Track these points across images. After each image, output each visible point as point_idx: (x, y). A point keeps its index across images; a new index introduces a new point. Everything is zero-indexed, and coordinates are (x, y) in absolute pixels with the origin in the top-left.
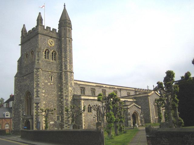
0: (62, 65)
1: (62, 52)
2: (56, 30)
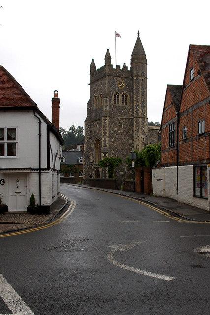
0: (133, 110)
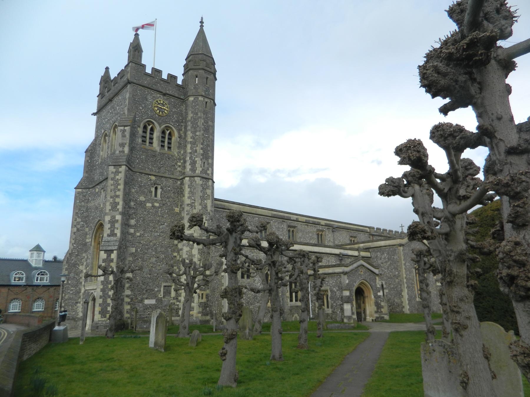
1: (187, 131)
2: (175, 78)
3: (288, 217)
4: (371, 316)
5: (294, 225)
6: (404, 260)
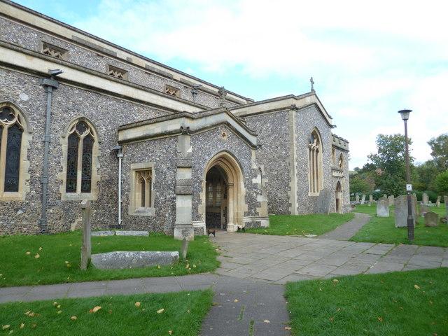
3: (110, 51)
4: (237, 220)
5: (121, 68)
6: (297, 131)
